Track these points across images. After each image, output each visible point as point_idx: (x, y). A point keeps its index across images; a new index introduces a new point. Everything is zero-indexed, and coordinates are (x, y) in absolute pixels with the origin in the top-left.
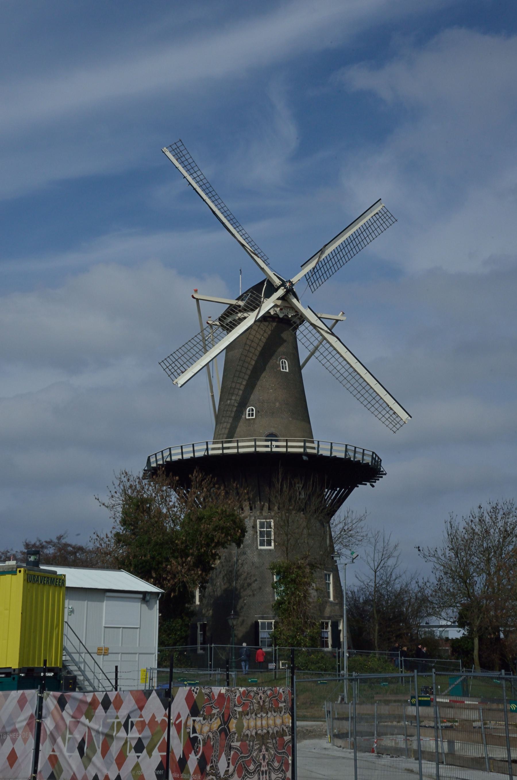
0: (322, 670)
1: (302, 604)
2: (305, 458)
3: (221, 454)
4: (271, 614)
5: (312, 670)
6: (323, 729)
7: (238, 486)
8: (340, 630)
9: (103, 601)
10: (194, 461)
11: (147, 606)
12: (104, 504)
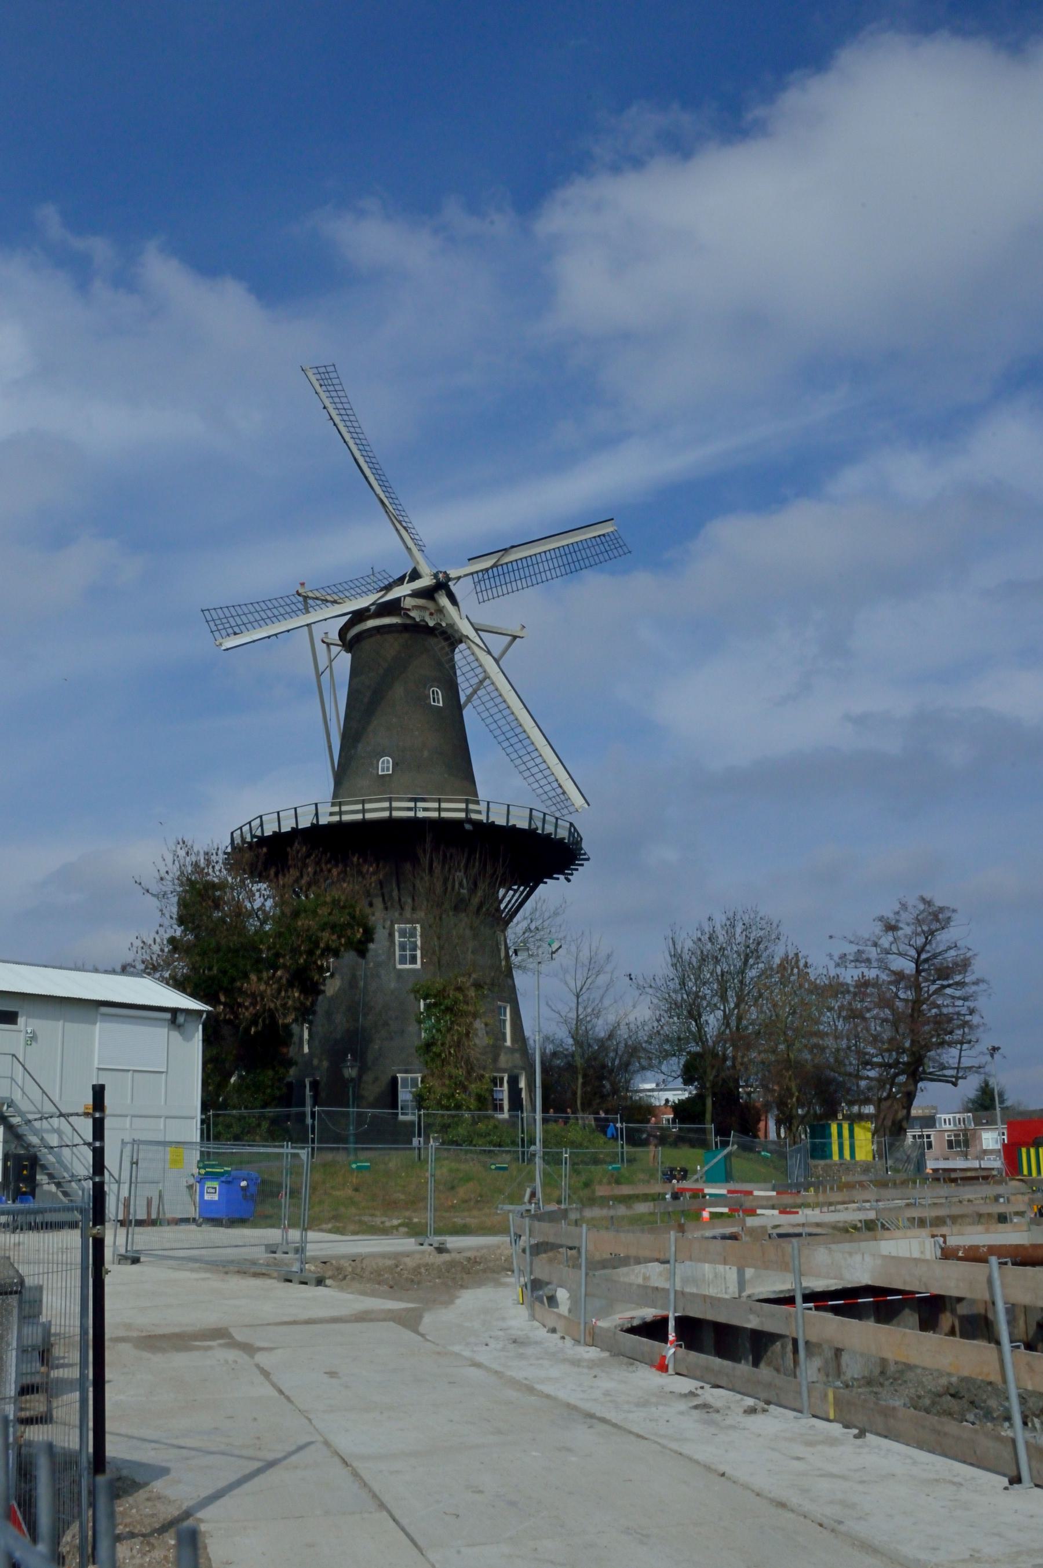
0: (495, 1146)
2: (468, 827)
5: (479, 1146)
6: (501, 1255)
8: (521, 1089)
9: (95, 1023)
10: (295, 831)
11: (181, 1034)
12: (148, 891)
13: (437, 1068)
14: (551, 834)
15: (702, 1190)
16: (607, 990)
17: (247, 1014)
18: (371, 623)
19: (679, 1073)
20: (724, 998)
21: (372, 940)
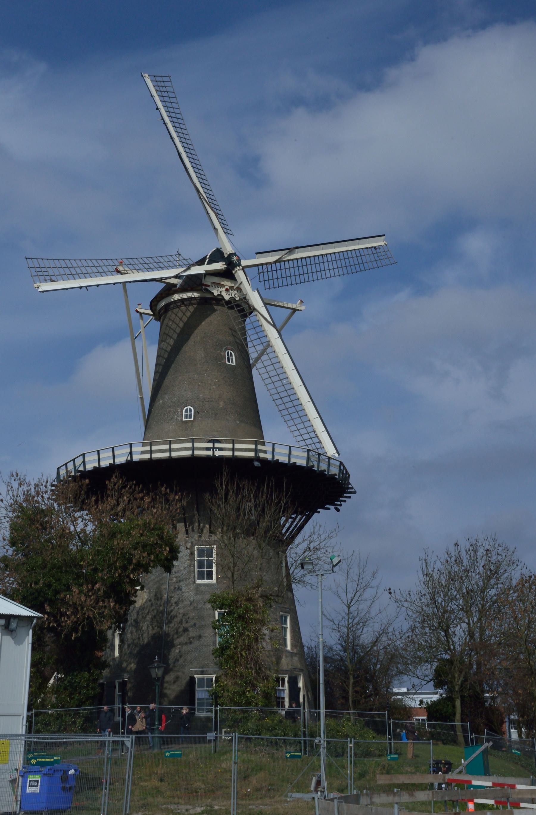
1: (252, 648)
2: (256, 464)
3: (148, 458)
4: (212, 666)
7: (168, 490)
8: (300, 688)
10: (113, 467)
13: (230, 669)
14: (325, 471)
15: (470, 782)
16: (373, 602)
17: (67, 622)
18: (176, 297)
19: (431, 678)
20: (468, 612)
21: (176, 558)
